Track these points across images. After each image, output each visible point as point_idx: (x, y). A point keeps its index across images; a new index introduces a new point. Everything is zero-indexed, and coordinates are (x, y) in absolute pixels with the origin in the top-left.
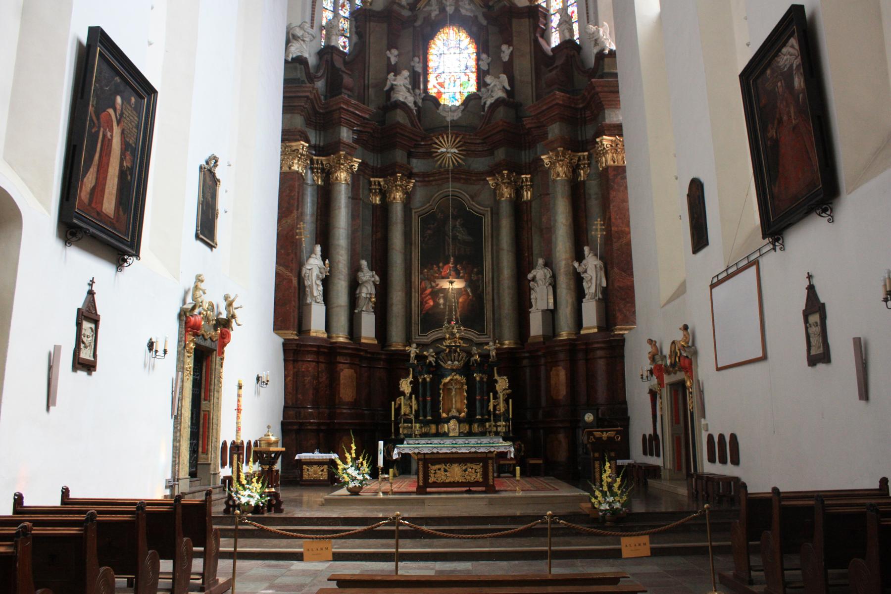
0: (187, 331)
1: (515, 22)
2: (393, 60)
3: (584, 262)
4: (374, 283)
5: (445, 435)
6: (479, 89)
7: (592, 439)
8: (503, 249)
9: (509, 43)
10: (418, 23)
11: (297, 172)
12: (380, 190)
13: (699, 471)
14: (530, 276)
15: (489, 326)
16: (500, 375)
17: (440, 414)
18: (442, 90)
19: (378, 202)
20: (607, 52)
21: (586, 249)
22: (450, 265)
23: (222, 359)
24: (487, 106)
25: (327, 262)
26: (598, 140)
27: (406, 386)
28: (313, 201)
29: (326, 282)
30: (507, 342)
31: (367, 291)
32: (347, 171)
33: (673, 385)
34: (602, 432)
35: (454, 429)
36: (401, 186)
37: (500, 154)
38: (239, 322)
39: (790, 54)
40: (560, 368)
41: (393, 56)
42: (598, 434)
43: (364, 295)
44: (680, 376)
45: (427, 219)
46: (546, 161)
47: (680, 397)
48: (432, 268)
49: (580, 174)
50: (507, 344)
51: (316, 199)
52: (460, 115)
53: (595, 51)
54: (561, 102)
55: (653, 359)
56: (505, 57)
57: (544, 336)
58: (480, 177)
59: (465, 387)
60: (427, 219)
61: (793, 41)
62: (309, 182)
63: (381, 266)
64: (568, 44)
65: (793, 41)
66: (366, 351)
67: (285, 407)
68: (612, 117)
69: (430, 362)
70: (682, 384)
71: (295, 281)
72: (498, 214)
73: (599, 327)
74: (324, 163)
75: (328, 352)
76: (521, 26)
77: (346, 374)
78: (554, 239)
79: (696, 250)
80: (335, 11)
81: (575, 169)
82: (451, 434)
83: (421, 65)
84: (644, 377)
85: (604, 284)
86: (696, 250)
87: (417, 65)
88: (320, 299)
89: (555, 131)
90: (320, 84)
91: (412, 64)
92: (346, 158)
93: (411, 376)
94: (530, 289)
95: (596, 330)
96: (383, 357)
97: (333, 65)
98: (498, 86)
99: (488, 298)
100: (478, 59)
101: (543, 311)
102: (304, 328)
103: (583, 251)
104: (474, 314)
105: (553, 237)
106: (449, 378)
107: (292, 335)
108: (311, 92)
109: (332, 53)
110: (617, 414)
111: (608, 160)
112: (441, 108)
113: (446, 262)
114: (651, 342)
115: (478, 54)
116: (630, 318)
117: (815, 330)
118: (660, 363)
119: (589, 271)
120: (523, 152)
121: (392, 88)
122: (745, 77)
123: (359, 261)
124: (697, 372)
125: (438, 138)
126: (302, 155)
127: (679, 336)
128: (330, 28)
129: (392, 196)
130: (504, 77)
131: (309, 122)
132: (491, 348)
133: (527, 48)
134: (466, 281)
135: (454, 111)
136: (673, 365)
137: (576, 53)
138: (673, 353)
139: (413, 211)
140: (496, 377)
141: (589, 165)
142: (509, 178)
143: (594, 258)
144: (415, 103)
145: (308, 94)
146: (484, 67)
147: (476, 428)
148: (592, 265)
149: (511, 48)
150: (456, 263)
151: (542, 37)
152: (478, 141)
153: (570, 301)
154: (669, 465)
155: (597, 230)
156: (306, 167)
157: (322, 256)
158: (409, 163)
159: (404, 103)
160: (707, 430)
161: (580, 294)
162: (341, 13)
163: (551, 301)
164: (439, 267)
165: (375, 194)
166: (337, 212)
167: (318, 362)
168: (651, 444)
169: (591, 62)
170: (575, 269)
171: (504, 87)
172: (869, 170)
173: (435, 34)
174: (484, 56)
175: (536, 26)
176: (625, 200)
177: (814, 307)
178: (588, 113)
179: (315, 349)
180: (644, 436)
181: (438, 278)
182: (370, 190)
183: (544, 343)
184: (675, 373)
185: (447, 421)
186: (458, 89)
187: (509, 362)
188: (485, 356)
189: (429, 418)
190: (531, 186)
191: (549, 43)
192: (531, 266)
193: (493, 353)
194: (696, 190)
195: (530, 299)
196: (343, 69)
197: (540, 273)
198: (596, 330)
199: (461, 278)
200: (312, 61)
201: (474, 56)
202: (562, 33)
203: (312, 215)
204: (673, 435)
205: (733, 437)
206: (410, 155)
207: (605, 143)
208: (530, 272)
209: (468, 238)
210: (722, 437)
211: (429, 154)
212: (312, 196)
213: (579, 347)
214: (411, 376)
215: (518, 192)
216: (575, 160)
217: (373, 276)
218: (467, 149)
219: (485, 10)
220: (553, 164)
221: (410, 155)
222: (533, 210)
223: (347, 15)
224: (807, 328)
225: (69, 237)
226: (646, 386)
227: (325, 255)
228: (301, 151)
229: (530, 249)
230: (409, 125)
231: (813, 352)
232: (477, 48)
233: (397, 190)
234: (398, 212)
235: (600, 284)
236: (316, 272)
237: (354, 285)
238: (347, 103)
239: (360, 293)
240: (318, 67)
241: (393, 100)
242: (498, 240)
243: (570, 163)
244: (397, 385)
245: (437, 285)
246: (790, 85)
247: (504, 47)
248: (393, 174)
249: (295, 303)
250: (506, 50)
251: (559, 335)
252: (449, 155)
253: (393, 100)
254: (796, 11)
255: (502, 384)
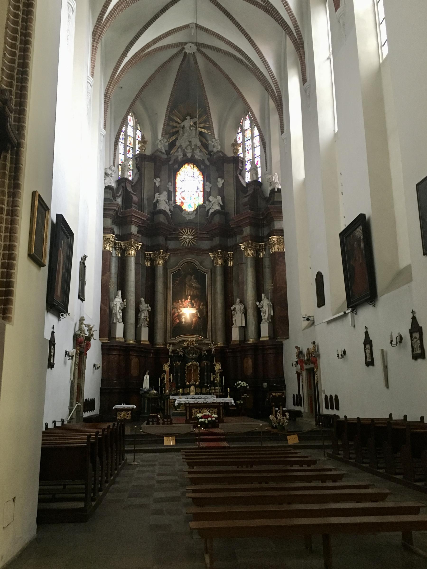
0: (77, 345)
1: (225, 165)
2: (157, 184)
3: (262, 302)
4: (148, 311)
5: (189, 394)
6: (204, 202)
7: (271, 396)
8: (217, 293)
9: (223, 178)
10: (171, 163)
11: (109, 251)
12: (151, 258)
13: (321, 413)
14: (232, 308)
15: (209, 334)
16: (216, 362)
17: (185, 383)
18: (184, 201)
19: (149, 265)
20: (276, 190)
21: (263, 295)
22: (188, 300)
23: (86, 357)
24: (210, 213)
25: (125, 300)
26: (270, 238)
27: (166, 367)
28: (115, 266)
29: (124, 311)
30: (219, 343)
31: (144, 315)
32: (135, 250)
33: (307, 370)
34: (276, 393)
35: (193, 391)
36: (162, 257)
37: (217, 241)
38: (95, 338)
39: (359, 232)
40: (249, 358)
41: (157, 182)
42: (274, 394)
43: (143, 317)
44: (312, 366)
45: (175, 275)
46: (242, 247)
47: (312, 378)
48: (178, 302)
49: (260, 254)
50: (220, 344)
51: (117, 264)
52: (194, 216)
53: (270, 188)
54: (251, 216)
55: (298, 356)
56: (220, 186)
57: (240, 341)
58: (205, 252)
59: (199, 368)
60: (175, 275)
61: (361, 227)
62: (114, 255)
63: (151, 301)
64: (255, 182)
65: (361, 227)
66: (145, 348)
67: (102, 380)
68: (277, 225)
69: (180, 355)
70: (313, 369)
71: (108, 311)
72: (215, 273)
73: (269, 337)
74: (122, 245)
75: (125, 349)
76: (229, 167)
77: (134, 361)
78: (245, 289)
79: (319, 306)
80: (125, 154)
81: (257, 252)
82: (191, 394)
83: (172, 187)
84: (294, 365)
85: (272, 314)
86: (319, 306)
87: (170, 187)
88: (121, 320)
89: (247, 231)
90: (119, 201)
91: (168, 186)
92: (135, 243)
93: (169, 362)
94: (232, 315)
95: (268, 339)
96: (152, 351)
97: (126, 188)
98: (215, 204)
99: (209, 319)
100: (204, 185)
101: (239, 327)
102: (112, 336)
103: (262, 296)
104: (201, 325)
105: (245, 287)
106: (190, 364)
107: (106, 340)
108: (117, 207)
109: (126, 182)
110: (280, 383)
111: (275, 249)
112: (184, 212)
113: (186, 299)
114: (297, 348)
115: (204, 181)
116: (286, 335)
117: (368, 351)
118: (302, 358)
119: (264, 307)
120: (229, 239)
121: (157, 201)
122: (342, 235)
123: (140, 299)
124: (320, 364)
125: (182, 230)
126: (111, 241)
127: (311, 346)
128: (124, 167)
129: (158, 262)
130: (219, 198)
131: (113, 222)
132: (212, 346)
133: (232, 181)
134: (197, 309)
135: (191, 214)
136: (308, 360)
137: (259, 187)
138: (308, 354)
139: (168, 270)
140: (215, 363)
141: (265, 249)
142: (221, 254)
143: (267, 300)
144: (170, 210)
145: (115, 208)
146: (208, 190)
147: (204, 390)
148: (266, 303)
149: (223, 181)
150: (191, 300)
151: (240, 174)
152: (204, 232)
153: (254, 322)
154: (306, 410)
155: (268, 285)
156: (112, 248)
157: (122, 297)
158: (166, 243)
159: (164, 211)
160: (324, 393)
161: (259, 319)
162: (128, 155)
163: (244, 322)
164: (182, 302)
165: (147, 261)
166: (129, 272)
167: (120, 355)
168: (298, 400)
169: (268, 194)
170: (257, 306)
171: (219, 203)
172: (388, 289)
173: (180, 169)
174: (207, 183)
175: (237, 168)
176: (284, 271)
177: (368, 342)
178: (265, 222)
179: (118, 348)
180: (294, 395)
181: (182, 307)
182: (145, 258)
183: (240, 345)
184: (309, 364)
185: (189, 386)
186: (193, 201)
187: (221, 354)
188: (209, 351)
189: (179, 385)
190: (233, 258)
191: (244, 178)
192: (232, 303)
193: (213, 350)
194: (320, 278)
195: (232, 320)
196: (132, 192)
197: (238, 306)
198: (268, 339)
199: (195, 307)
200: (114, 185)
201: (202, 183)
202: (252, 175)
203: (115, 273)
204: (308, 395)
205: (336, 396)
206: (167, 239)
207: (274, 239)
208: (232, 306)
209: (198, 286)
210: (331, 396)
211: (177, 239)
212: (115, 263)
213: (259, 347)
214: (169, 362)
215: (226, 261)
216: (258, 247)
217: (148, 307)
218: (198, 237)
219: (209, 156)
220: (246, 249)
221: (167, 239)
222: (234, 272)
223: (131, 156)
224: (365, 350)
225: (49, 309)
226: (294, 370)
227: (123, 297)
228: (111, 239)
229: (232, 292)
230: (167, 223)
231: (367, 361)
232: (204, 178)
233: (160, 259)
234: (160, 271)
235: (270, 315)
236: (119, 306)
237: (138, 311)
238: (135, 212)
239: (141, 316)
240: (118, 189)
241: (158, 209)
242: (215, 289)
243: (255, 248)
244: (162, 367)
245: (181, 311)
246: (359, 245)
247: (219, 180)
248: (159, 250)
249: (107, 323)
250: (220, 182)
251: (248, 341)
252: (188, 240)
253: (158, 209)
254: (362, 217)
255: (218, 367)
